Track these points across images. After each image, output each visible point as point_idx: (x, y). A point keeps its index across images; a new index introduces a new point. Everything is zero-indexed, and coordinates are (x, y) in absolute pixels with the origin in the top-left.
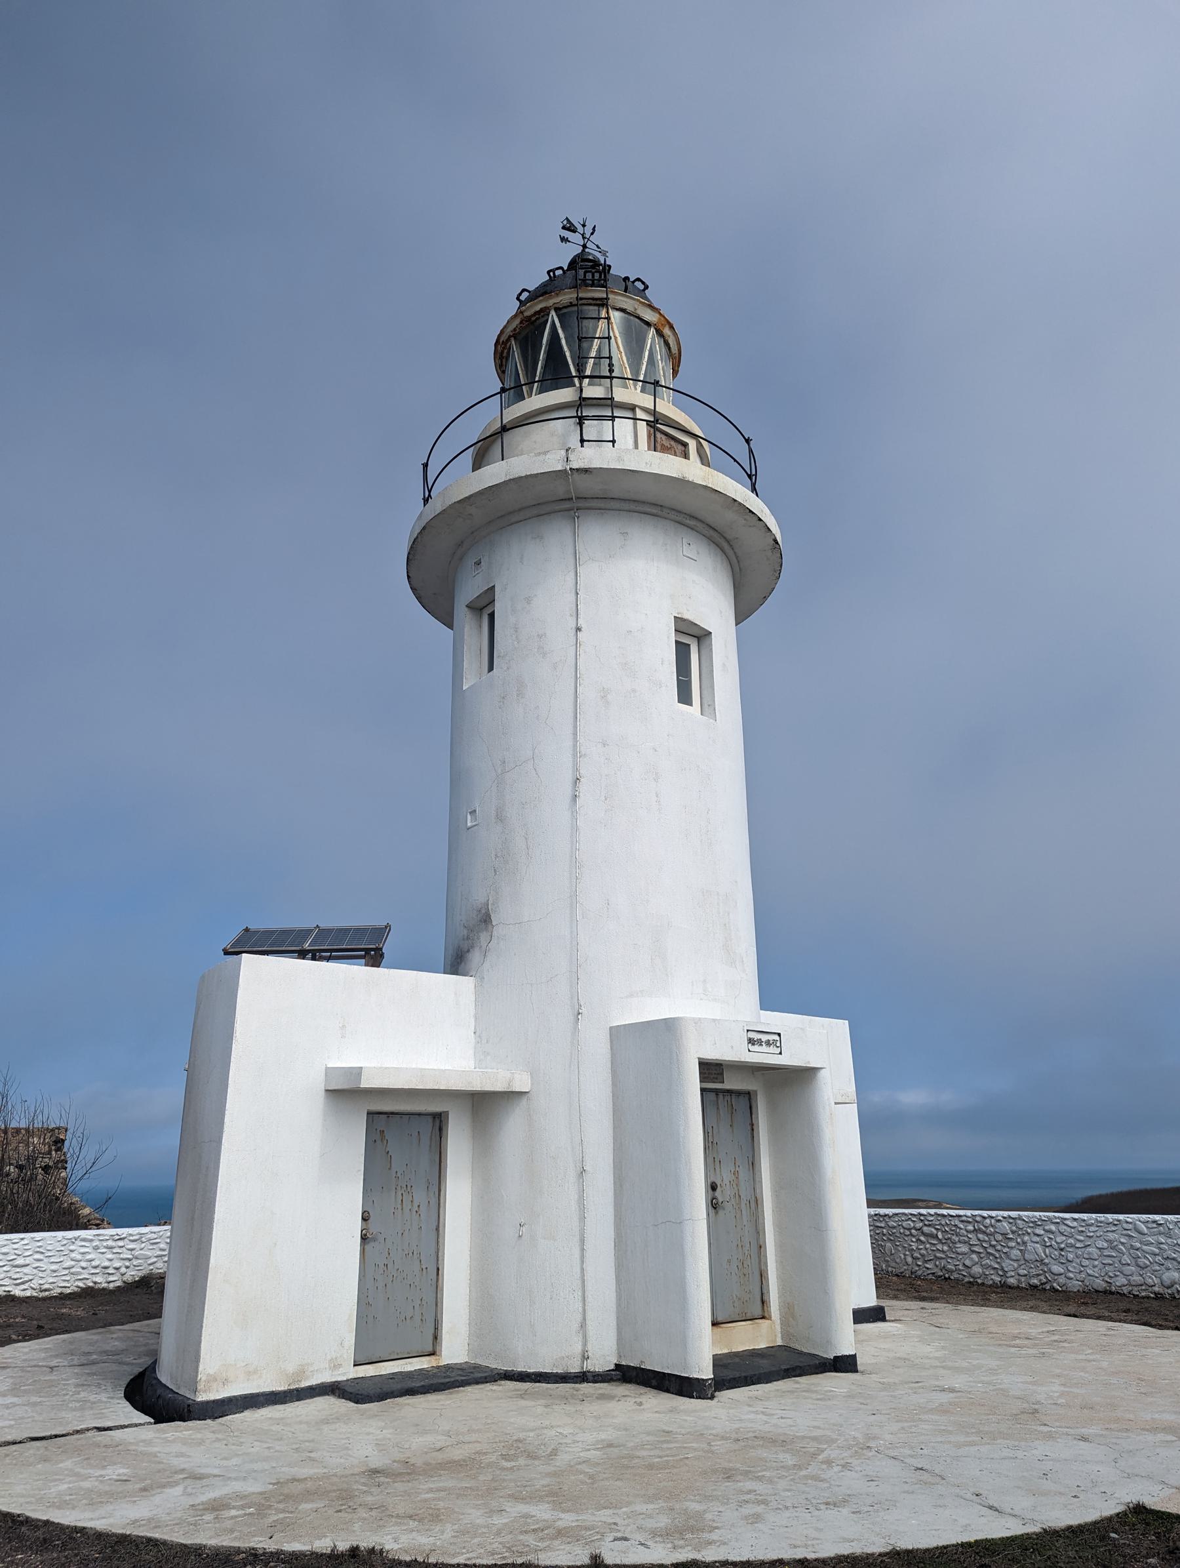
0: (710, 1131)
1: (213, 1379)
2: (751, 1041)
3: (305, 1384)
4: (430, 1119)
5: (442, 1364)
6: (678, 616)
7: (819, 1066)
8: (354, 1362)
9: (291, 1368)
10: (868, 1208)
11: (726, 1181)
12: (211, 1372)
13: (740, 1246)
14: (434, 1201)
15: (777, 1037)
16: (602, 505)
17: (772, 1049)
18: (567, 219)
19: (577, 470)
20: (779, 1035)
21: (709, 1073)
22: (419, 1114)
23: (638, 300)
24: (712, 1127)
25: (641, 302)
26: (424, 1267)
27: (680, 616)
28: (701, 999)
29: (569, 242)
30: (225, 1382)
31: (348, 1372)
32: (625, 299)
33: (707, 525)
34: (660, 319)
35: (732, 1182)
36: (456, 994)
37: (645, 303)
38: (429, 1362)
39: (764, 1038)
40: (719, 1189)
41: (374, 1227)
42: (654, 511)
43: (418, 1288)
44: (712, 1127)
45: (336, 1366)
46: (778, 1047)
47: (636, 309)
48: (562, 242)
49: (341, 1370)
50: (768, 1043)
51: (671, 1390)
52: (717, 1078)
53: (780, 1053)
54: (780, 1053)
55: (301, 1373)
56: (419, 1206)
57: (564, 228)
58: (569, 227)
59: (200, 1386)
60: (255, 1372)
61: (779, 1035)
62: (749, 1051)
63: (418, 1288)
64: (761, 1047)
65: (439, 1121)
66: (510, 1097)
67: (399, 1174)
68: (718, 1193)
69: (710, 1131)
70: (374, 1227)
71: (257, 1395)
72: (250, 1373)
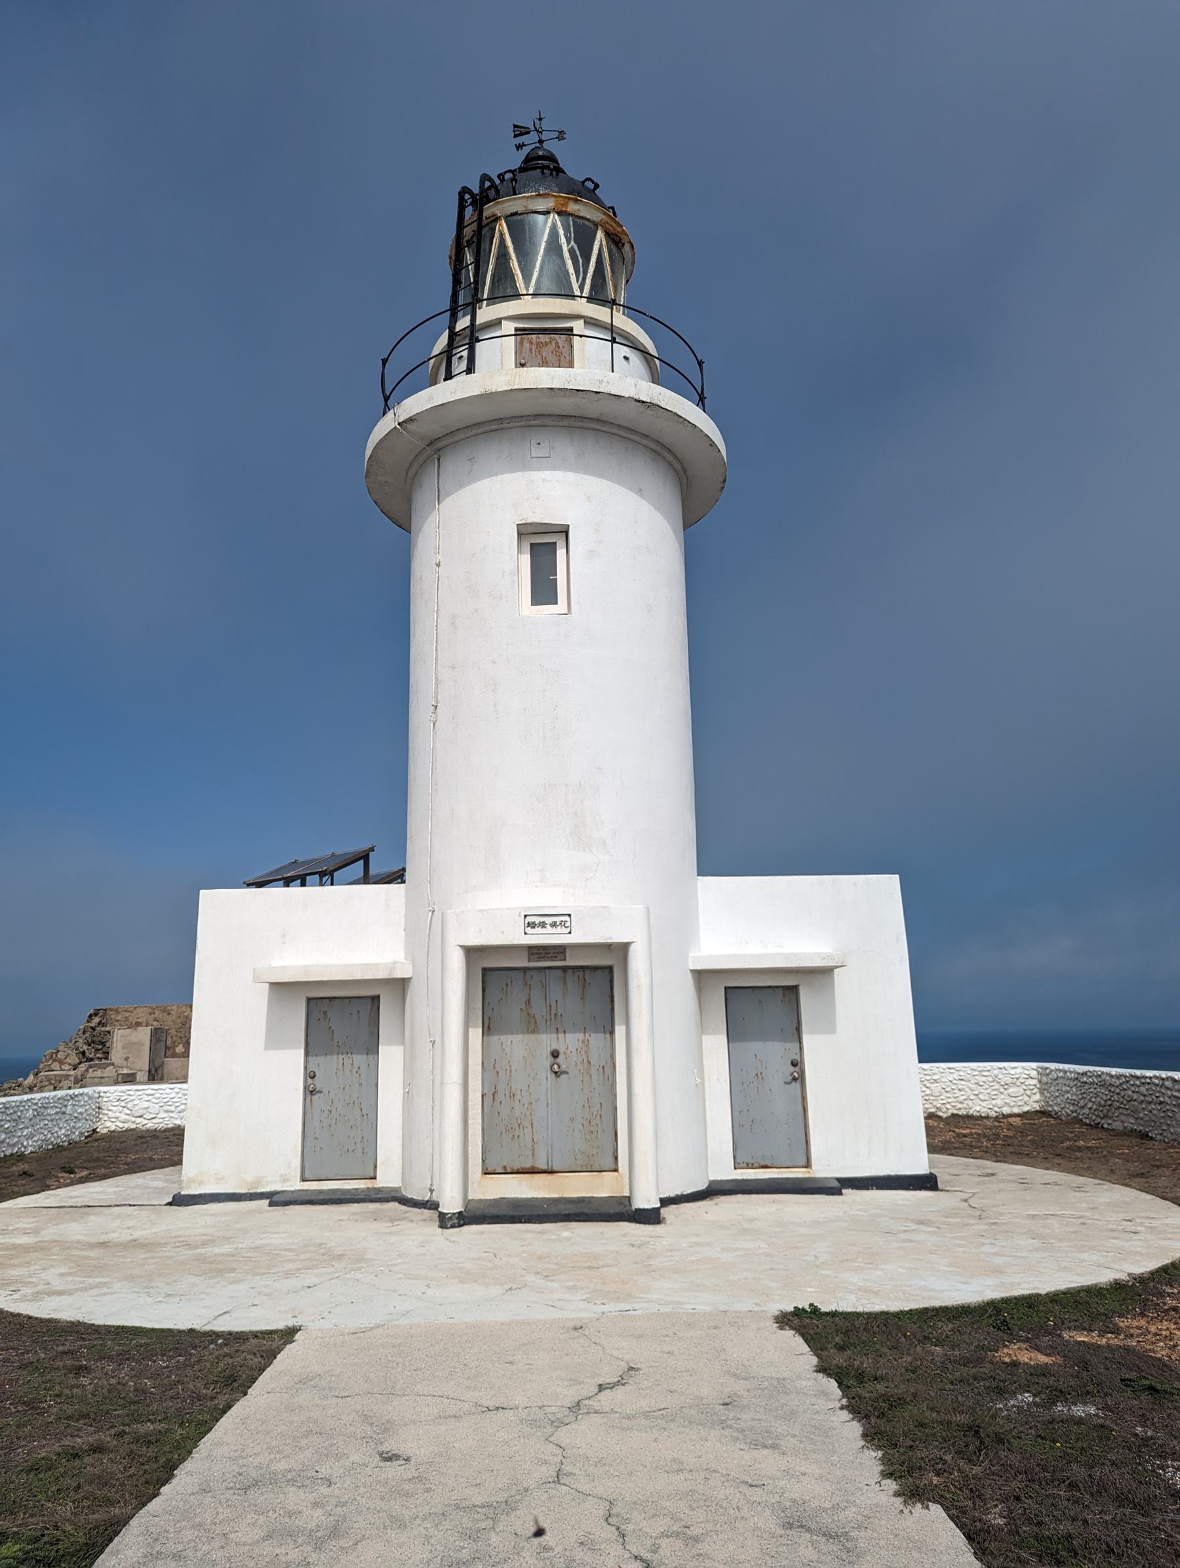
0: (553, 1004)
1: (191, 1181)
2: (532, 925)
3: (259, 1190)
4: (369, 1001)
5: (376, 1186)
6: (520, 523)
7: (629, 941)
8: (483, 1170)
9: (250, 1178)
10: (920, 1061)
11: (572, 1048)
12: (191, 1175)
13: (587, 1106)
14: (609, 1044)
15: (567, 918)
16: (452, 440)
17: (559, 930)
18: (515, 126)
19: (404, 422)
20: (570, 915)
21: (546, 953)
22: (359, 998)
23: (524, 197)
24: (557, 1001)
25: (528, 197)
26: (365, 1114)
27: (523, 522)
28: (537, 887)
29: (525, 145)
30: (201, 1183)
31: (295, 1185)
32: (511, 203)
33: (558, 415)
34: (556, 201)
35: (579, 1050)
36: (386, 900)
37: (531, 196)
38: (366, 1184)
39: (548, 920)
40: (561, 1056)
41: (319, 1083)
42: (494, 427)
43: (359, 1129)
44: (557, 1001)
45: (285, 1180)
46: (567, 927)
47: (526, 207)
48: (518, 150)
49: (289, 1183)
50: (554, 925)
51: (643, 1221)
52: (556, 957)
53: (570, 933)
54: (570, 933)
55: (258, 1182)
56: (359, 1068)
57: (516, 136)
58: (520, 131)
59: (184, 1185)
60: (223, 1178)
61: (570, 915)
62: (526, 933)
63: (359, 1129)
64: (544, 929)
65: (376, 999)
66: (822, 974)
67: (340, 1044)
68: (560, 1060)
69: (553, 1004)
70: (319, 1083)
71: (221, 1194)
72: (218, 1180)
